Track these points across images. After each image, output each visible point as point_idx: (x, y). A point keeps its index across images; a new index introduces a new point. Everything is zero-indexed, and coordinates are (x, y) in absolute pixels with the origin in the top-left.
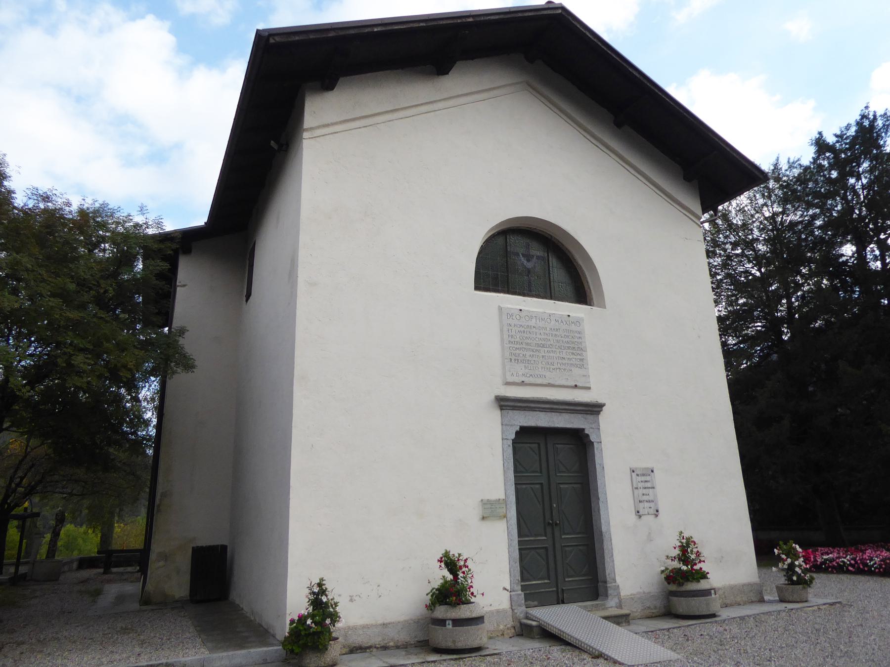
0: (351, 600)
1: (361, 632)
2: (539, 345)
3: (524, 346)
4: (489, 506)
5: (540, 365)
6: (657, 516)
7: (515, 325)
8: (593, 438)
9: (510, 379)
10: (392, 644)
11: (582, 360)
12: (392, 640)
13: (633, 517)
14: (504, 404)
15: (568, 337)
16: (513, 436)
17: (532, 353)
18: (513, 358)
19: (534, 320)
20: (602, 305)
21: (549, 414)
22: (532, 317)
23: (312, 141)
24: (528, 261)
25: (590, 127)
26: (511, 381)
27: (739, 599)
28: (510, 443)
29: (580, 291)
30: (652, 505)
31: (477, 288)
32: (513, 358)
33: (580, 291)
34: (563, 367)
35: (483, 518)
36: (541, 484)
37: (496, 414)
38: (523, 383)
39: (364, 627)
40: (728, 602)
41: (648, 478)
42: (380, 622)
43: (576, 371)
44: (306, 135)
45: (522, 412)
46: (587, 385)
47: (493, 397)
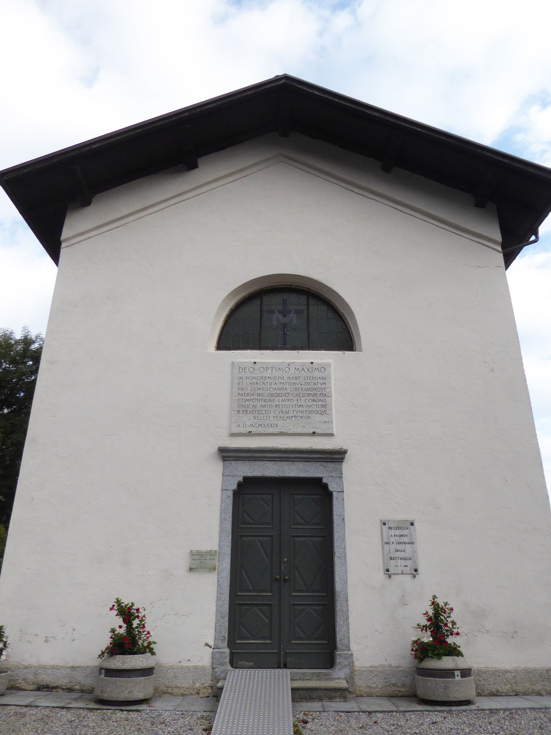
0: (46, 641)
1: (50, 672)
2: (272, 395)
3: (256, 397)
4: (198, 557)
5: (272, 414)
7: (247, 378)
9: (236, 430)
10: (77, 687)
12: (79, 683)
13: (381, 576)
15: (308, 384)
16: (235, 487)
17: (263, 403)
18: (241, 409)
19: (269, 371)
20: (361, 350)
21: (279, 463)
22: (267, 368)
23: (66, 249)
24: (285, 316)
25: (350, 178)
26: (237, 432)
27: (538, 687)
28: (230, 493)
29: (342, 336)
30: (409, 563)
32: (241, 409)
33: (342, 336)
34: (301, 415)
35: (191, 569)
36: (271, 536)
37: (218, 467)
38: (250, 434)
39: (53, 667)
40: (520, 689)
41: (405, 532)
42: (70, 665)
43: (317, 418)
44: (63, 245)
45: (247, 463)
46: (329, 432)
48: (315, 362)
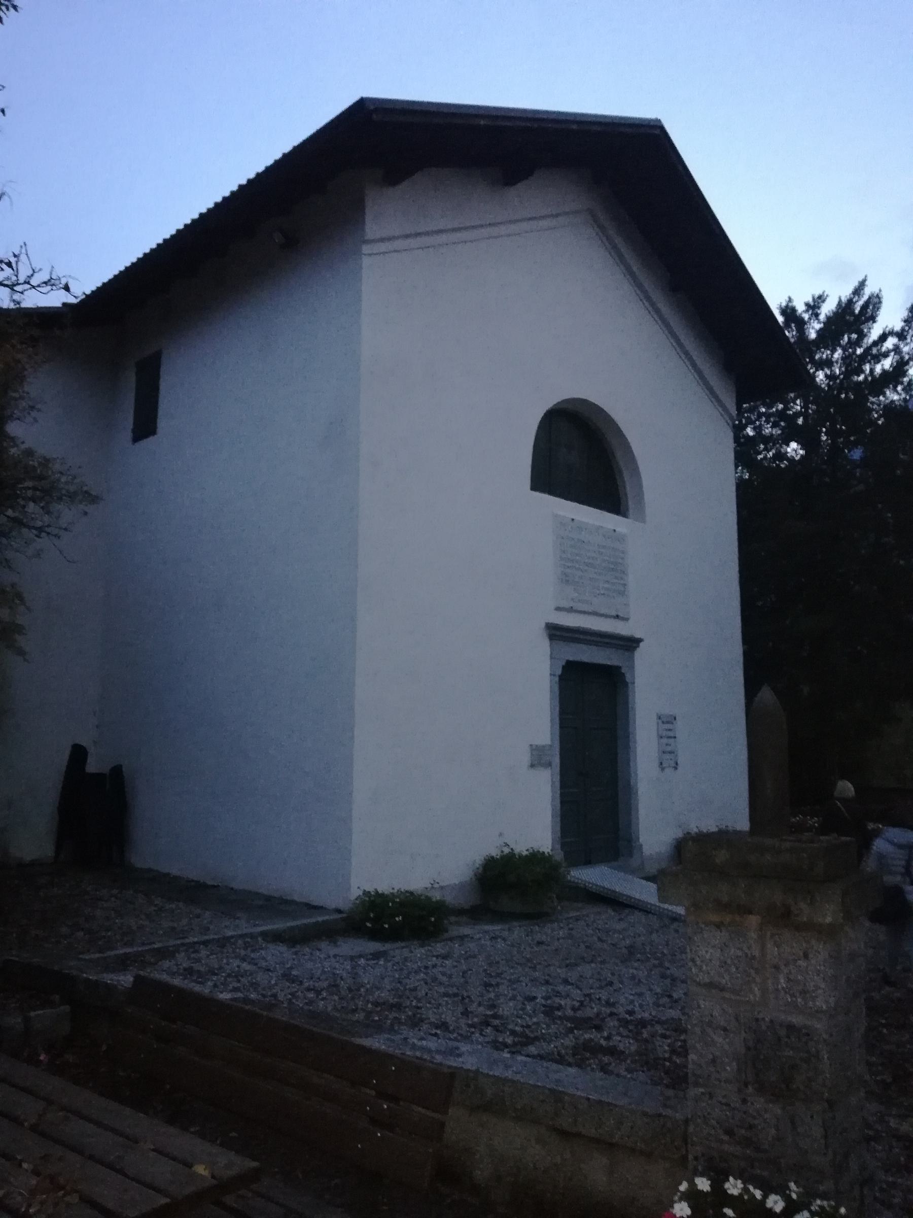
2: (587, 565)
6: (676, 768)
8: (628, 678)
11: (625, 585)
14: (556, 633)
20: (641, 517)
28: (557, 679)
30: (672, 756)
31: (533, 488)
37: (544, 645)
47: (543, 625)
48: (617, 530)
